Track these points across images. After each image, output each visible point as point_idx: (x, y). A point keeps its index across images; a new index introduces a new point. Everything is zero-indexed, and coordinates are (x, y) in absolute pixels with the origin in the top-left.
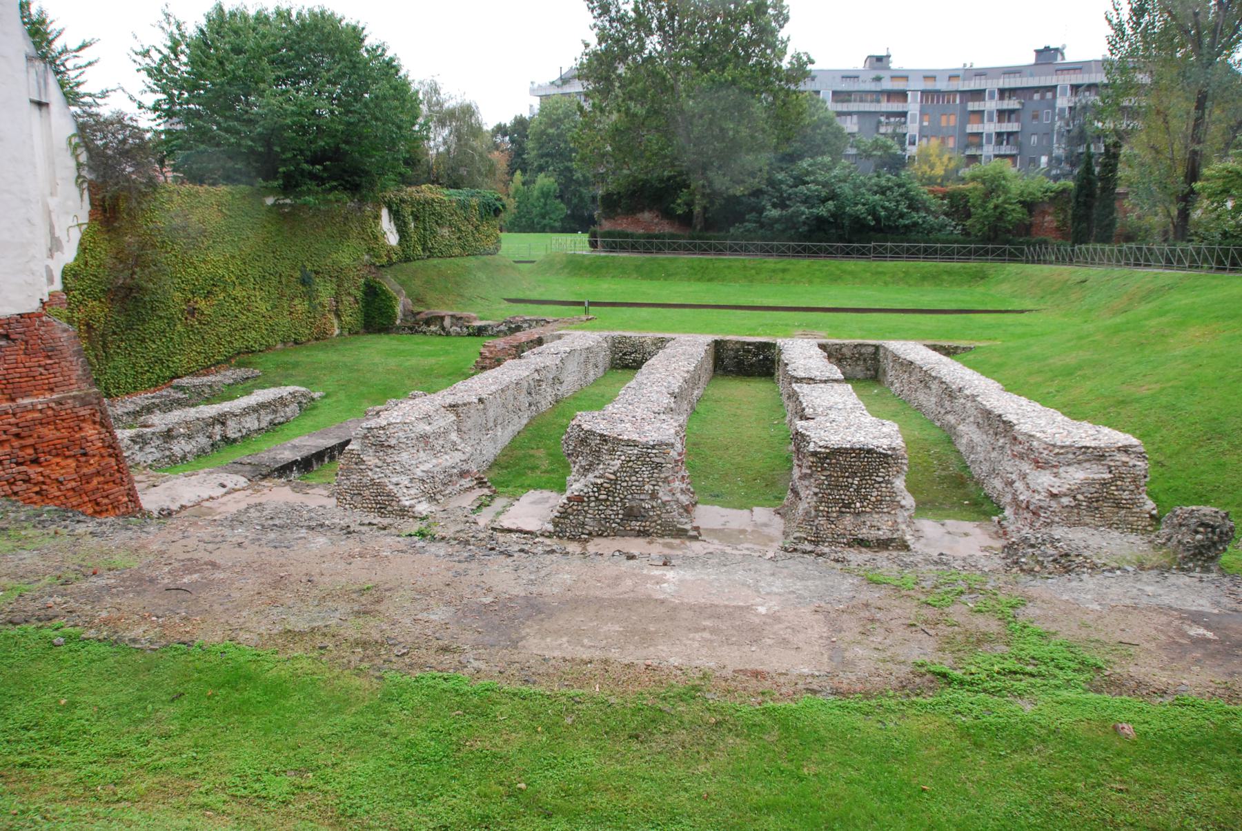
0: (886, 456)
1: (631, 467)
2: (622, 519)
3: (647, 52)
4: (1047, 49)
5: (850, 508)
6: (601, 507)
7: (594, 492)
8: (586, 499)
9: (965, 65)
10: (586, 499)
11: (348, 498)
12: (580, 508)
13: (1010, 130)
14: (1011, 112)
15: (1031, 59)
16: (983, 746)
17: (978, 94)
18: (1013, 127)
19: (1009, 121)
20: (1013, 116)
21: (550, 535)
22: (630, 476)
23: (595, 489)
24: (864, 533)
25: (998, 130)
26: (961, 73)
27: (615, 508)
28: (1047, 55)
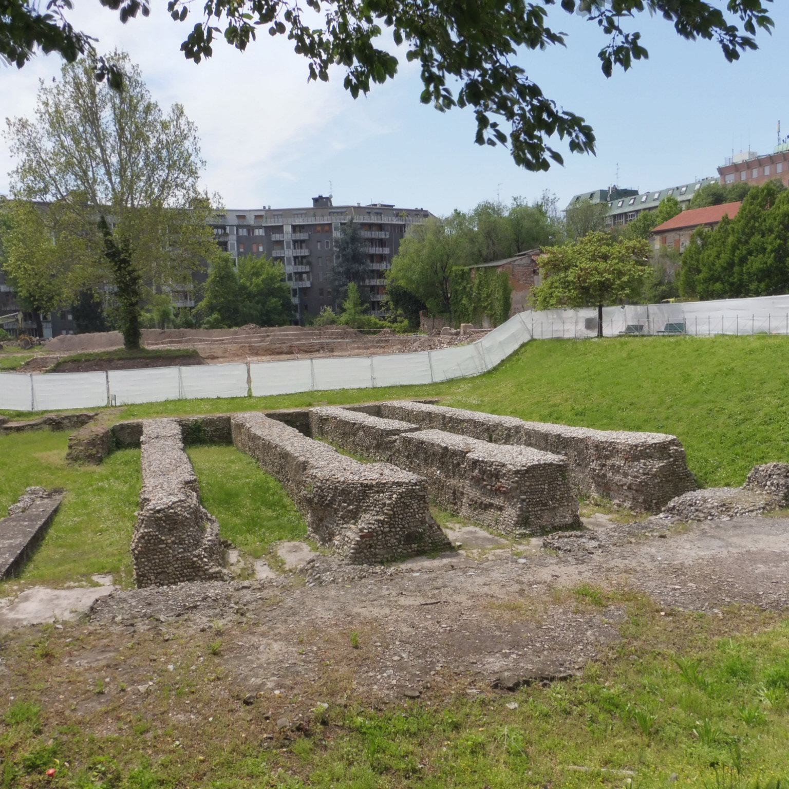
0: (560, 466)
1: (403, 502)
2: (403, 545)
3: (226, 9)
4: (321, 197)
5: (546, 506)
6: (387, 538)
7: (380, 527)
8: (375, 534)
9: (264, 207)
10: (375, 534)
11: (152, 578)
12: (371, 542)
13: (303, 254)
14: (302, 241)
15: (310, 204)
16: (285, 527)
17: (279, 229)
18: (304, 252)
19: (301, 248)
20: (304, 245)
21: (351, 564)
22: (404, 510)
23: (380, 525)
24: (558, 521)
25: (295, 255)
26: (263, 213)
27: (397, 536)
28: (321, 202)
